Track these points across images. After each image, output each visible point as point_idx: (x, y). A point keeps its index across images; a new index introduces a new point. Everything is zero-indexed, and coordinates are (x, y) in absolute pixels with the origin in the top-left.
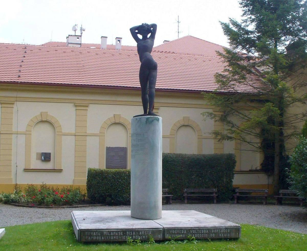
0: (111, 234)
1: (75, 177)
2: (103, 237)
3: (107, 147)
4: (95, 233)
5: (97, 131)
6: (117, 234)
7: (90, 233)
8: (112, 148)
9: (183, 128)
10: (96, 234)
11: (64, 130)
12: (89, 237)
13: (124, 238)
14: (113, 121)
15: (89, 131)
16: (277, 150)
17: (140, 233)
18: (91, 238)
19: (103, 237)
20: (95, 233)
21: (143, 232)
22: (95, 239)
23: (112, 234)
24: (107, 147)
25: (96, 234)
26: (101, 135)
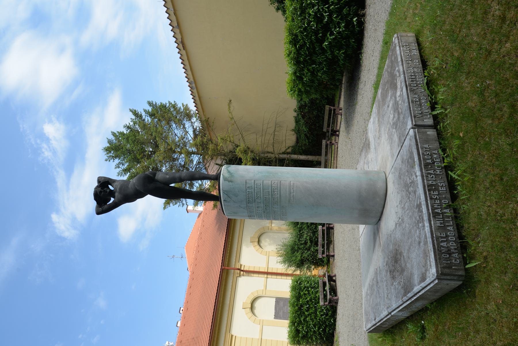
0: (439, 212)
1: (332, 279)
2: (449, 228)
3: (274, 318)
4: (442, 244)
5: (258, 327)
6: (438, 202)
7: (444, 253)
8: (275, 313)
9: (256, 311)
10: (442, 241)
11: (262, 288)
12: (454, 255)
13: (443, 189)
14: (249, 310)
15: (257, 336)
16: (285, 156)
17: (430, 161)
18: (453, 253)
19: (449, 228)
20: (442, 244)
21: (426, 157)
22: (455, 244)
23: (438, 211)
24: (274, 318)
25: (444, 241)
26: (262, 324)
